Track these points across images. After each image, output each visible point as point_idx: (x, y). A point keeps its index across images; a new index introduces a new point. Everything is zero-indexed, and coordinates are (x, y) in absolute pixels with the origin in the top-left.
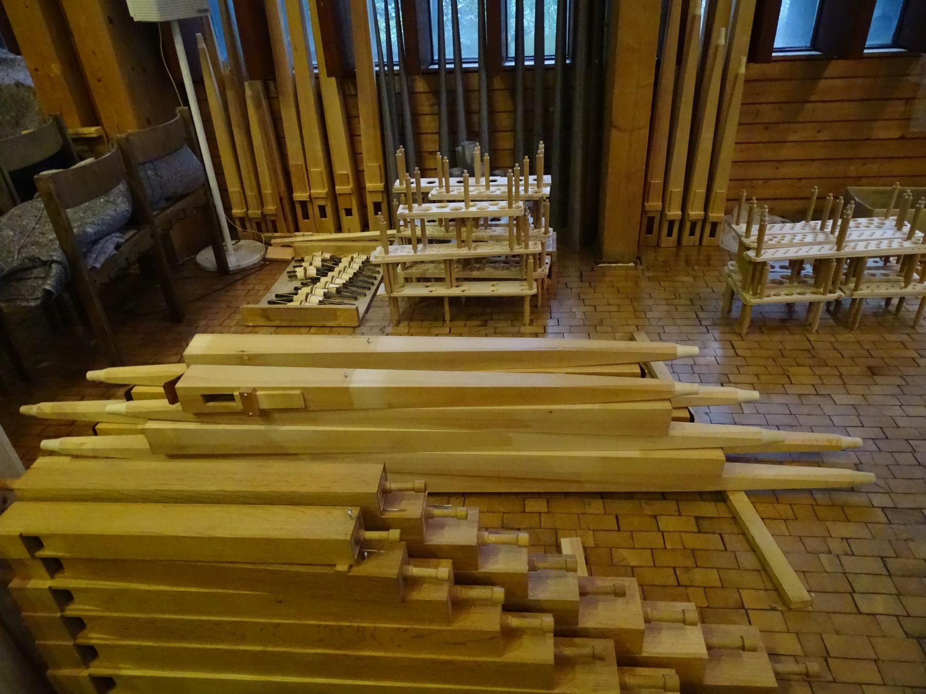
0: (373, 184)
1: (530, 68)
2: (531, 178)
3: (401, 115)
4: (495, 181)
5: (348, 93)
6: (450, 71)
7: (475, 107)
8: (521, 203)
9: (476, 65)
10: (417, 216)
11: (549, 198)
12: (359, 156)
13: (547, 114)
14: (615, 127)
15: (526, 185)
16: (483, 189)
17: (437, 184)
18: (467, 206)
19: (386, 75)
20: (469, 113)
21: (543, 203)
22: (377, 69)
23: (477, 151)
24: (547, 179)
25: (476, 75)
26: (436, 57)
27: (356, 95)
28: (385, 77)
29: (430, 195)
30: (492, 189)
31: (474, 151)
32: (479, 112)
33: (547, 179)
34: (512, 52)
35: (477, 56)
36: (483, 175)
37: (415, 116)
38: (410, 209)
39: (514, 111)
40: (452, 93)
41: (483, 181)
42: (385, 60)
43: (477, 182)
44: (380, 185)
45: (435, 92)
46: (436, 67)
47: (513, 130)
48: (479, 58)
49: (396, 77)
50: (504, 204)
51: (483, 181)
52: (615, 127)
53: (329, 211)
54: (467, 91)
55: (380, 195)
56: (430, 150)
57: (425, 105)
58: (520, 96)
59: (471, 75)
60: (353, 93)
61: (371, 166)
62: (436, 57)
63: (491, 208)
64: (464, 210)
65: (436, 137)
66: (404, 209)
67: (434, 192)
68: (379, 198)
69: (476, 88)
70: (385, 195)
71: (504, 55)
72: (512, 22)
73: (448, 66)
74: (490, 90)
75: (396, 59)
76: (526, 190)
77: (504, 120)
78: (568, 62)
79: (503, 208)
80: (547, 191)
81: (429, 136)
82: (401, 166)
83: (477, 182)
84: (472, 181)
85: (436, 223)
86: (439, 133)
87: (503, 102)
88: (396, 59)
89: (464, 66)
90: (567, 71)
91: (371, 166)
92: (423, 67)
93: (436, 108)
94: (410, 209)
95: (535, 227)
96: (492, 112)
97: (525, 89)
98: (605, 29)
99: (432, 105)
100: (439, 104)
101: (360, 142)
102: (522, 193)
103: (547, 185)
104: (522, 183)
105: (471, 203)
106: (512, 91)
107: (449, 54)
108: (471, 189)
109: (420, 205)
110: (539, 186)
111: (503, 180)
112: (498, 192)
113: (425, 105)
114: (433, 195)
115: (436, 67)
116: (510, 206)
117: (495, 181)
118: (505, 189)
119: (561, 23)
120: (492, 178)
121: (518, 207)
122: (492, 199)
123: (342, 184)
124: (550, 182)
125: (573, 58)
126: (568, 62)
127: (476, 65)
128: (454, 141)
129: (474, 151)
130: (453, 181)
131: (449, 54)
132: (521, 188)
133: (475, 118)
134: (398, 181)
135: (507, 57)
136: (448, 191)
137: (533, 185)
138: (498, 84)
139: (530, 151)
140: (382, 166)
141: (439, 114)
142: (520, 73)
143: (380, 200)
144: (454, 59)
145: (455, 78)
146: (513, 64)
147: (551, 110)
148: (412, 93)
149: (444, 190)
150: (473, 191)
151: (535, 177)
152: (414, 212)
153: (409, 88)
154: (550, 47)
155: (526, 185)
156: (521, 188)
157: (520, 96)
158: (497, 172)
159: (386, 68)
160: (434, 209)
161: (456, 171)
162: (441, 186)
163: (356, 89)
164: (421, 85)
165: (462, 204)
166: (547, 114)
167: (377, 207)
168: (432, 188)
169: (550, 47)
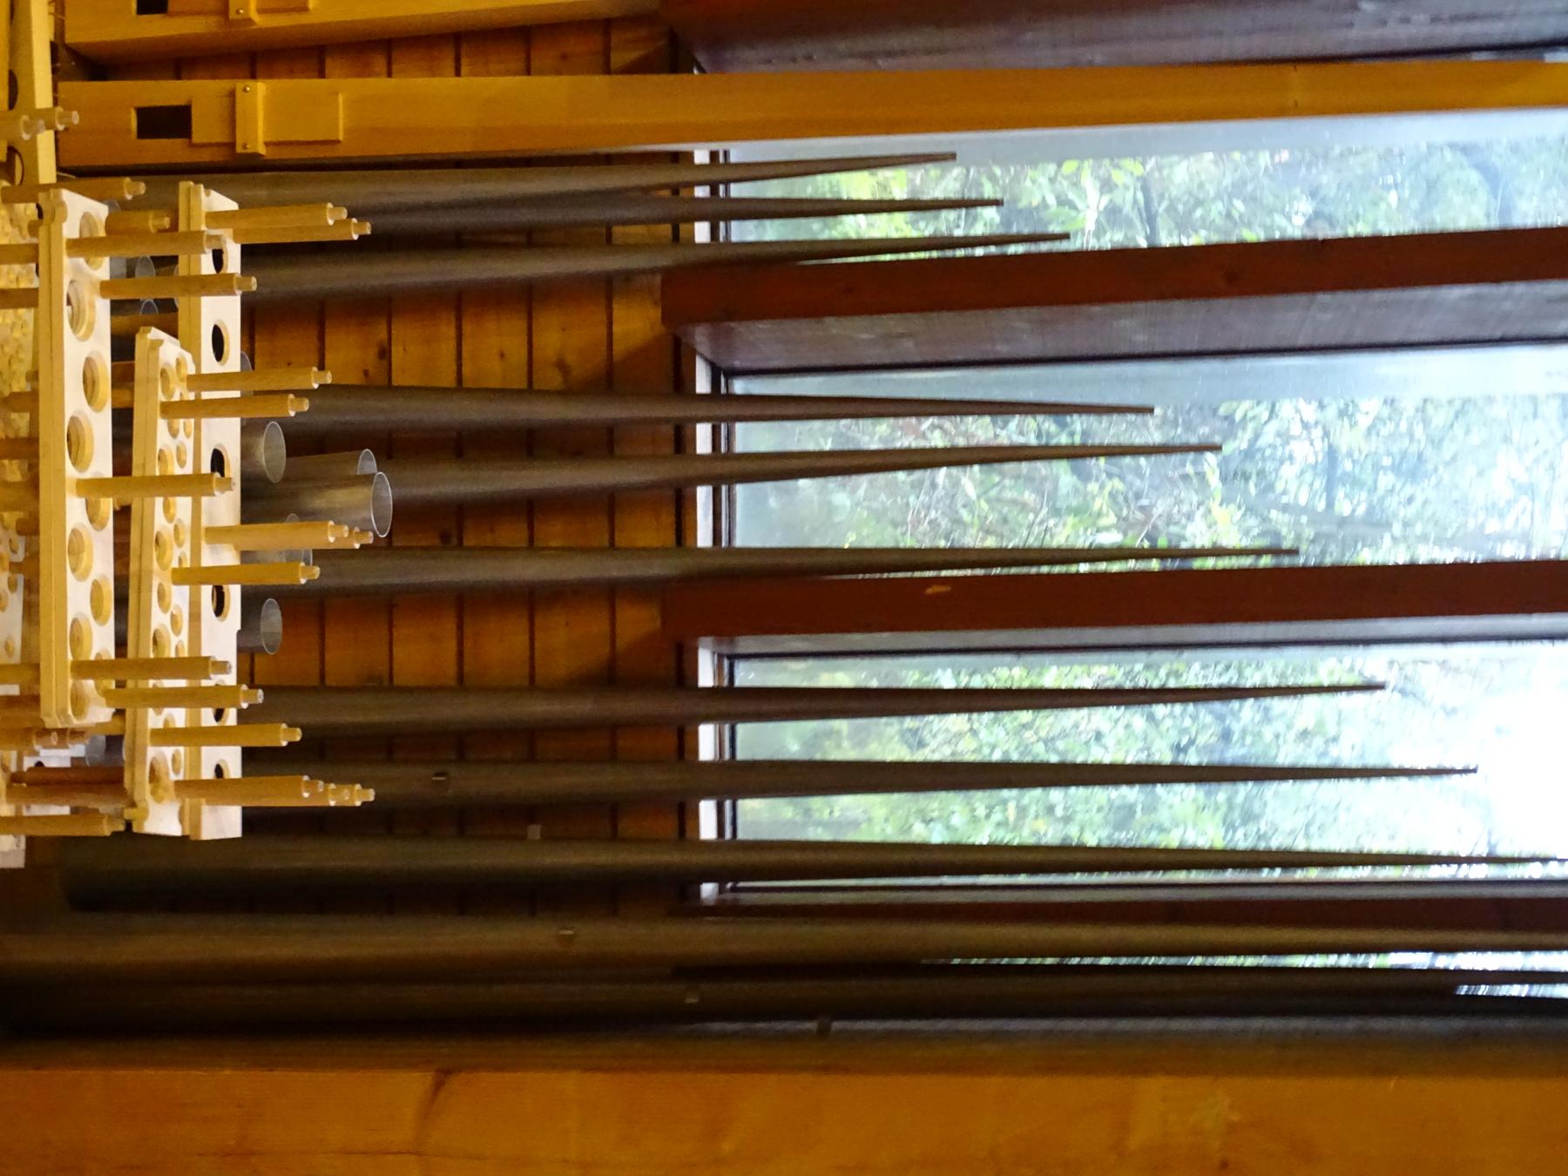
0: (263, 111)
1: (686, 743)
2: (231, 758)
3: (531, 239)
4: (219, 609)
5: (616, 38)
6: (682, 440)
7: (554, 532)
8: (99, 714)
9: (704, 538)
10: (52, 281)
11: (129, 836)
12: (380, 62)
13: (512, 816)
14: (438, 1086)
15: (193, 736)
16: (179, 555)
17: (210, 365)
18: (91, 489)
19: (675, 190)
20: (530, 507)
21: (105, 807)
22: (701, 156)
23: (333, 536)
24: (224, 822)
25: (669, 539)
26: (740, 386)
27: (607, 70)
28: (665, 183)
29: (155, 333)
30: (180, 596)
31: (349, 517)
32: (532, 547)
33: (224, 822)
34: (748, 675)
35: (739, 542)
36: (246, 556)
37: (527, 298)
38: (83, 246)
39: (532, 686)
40: (603, 442)
41: (227, 557)
42: (738, 190)
43: (217, 534)
44: (257, 137)
45: (609, 379)
46: (703, 385)
47: (461, 684)
48: (733, 551)
49: (666, 229)
50: (101, 642)
51: (227, 557)
52: (438, 1086)
53: (164, 92)
54: (609, 503)
55: (219, 136)
56: (397, 353)
57: (564, 337)
58: (583, 707)
59: (668, 519)
60: (618, 59)
61: (339, 108)
62: (740, 386)
63: (80, 592)
64: (71, 471)
65: (448, 380)
66: (86, 217)
67: (170, 350)
68: (205, 128)
69: (621, 540)
70: (217, 156)
71: (746, 644)
72: (945, 675)
73: (703, 432)
74: (611, 593)
75: (744, 232)
76: (167, 735)
77: (502, 644)
78: (708, 890)
79: (77, 640)
80: (163, 820)
81: (447, 348)
82: (285, 225)
83: (217, 534)
84: (224, 506)
85: (1502, 504)
86: (389, 389)
87: (568, 641)
88: (744, 232)
89: (703, 494)
90: (673, 892)
91: (339, 108)
92: (701, 337)
93: (554, 380)
94: (83, 246)
95: (15, 779)
96: (533, 600)
97: (614, 728)
98: (811, 1025)
99: (562, 366)
100: (569, 392)
101: (433, 72)
102: (154, 719)
103: (190, 817)
104: (207, 718)
105: (108, 506)
106: (609, 677)
107: (753, 437)
108: (183, 505)
109: (105, 288)
110: (190, 787)
111: (221, 638)
112: (159, 619)
113: (564, 337)
114: (157, 344)
115: (703, 385)
116: (85, 668)
117: (219, 609)
118: (177, 644)
119: (908, 857)
120: (234, 594)
121: (79, 702)
122: (123, 598)
123: (270, 100)
124: (209, 832)
125: (719, 910)
126: (708, 890)
127: (704, 538)
128: (393, 447)
129: (349, 517)
130: (225, 433)
131: (753, 437)
132: (179, 717)
133: (512, 533)
134: (232, 206)
135: (733, 658)
136: (169, 410)
137: (196, 763)
138: (636, 622)
139: (318, 752)
140: (340, 152)
141: (530, 391)
142: (672, 706)
143: (197, 137)
144: (731, 456)
145: (655, 458)
146: (706, 679)
147: (535, 831)
148: (608, 287)
149: (180, 393)
150: (166, 517)
151: (234, 770)
152: (70, 266)
153: (628, 276)
154: (763, 817)
155: (193, 736)
156: (179, 717)
157: (583, 707)
158: (273, 618)
159: (701, 192)
160: (86, 345)
161: (272, 453)
162: (199, 381)
163: (629, 70)
164: (636, 323)
165: (101, 463)
166: (512, 816)
167: (167, 122)
168: (192, 346)
169: (763, 817)
